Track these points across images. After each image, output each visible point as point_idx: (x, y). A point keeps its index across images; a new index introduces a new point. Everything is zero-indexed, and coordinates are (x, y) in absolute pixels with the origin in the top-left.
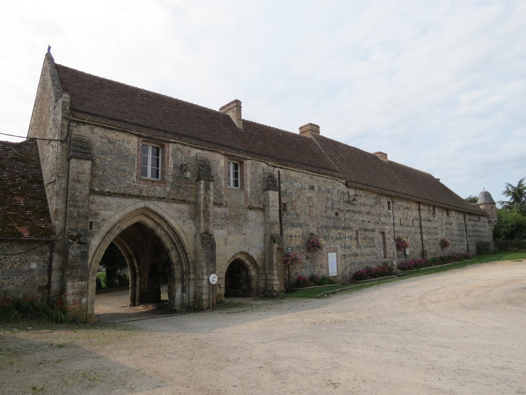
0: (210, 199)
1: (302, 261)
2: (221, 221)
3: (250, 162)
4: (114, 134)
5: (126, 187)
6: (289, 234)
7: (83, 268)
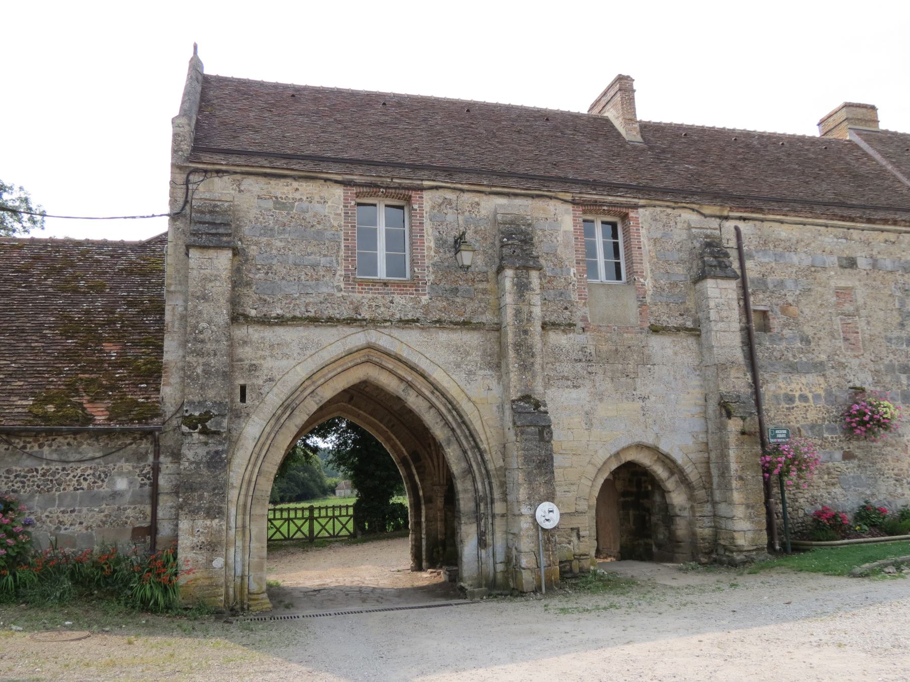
0: (531, 312)
1: (830, 464)
2: (573, 367)
3: (647, 213)
4: (289, 188)
5: (321, 303)
6: (783, 392)
7: (214, 489)
